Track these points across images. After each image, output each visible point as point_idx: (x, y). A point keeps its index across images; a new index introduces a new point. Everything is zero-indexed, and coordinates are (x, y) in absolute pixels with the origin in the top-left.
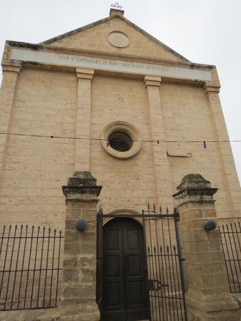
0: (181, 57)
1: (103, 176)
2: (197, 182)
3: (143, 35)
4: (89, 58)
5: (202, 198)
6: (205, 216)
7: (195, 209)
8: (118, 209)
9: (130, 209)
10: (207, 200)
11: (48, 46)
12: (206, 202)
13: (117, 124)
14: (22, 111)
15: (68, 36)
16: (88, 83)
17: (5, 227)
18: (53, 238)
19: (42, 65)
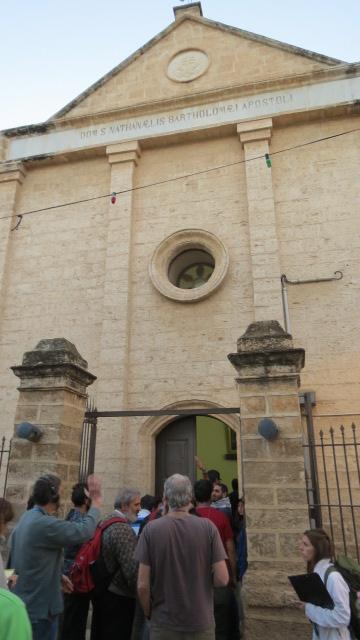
0: (323, 59)
1: (153, 339)
2: (261, 339)
3: (238, 39)
4: (132, 121)
5: (268, 372)
6: (270, 412)
7: (250, 394)
8: (180, 399)
9: (202, 398)
10: (277, 375)
11: (65, 119)
12: (275, 379)
13: (181, 236)
14: (26, 243)
15: (96, 90)
16: (129, 169)
17: (4, 439)
18: (342, 447)
19: (52, 157)
